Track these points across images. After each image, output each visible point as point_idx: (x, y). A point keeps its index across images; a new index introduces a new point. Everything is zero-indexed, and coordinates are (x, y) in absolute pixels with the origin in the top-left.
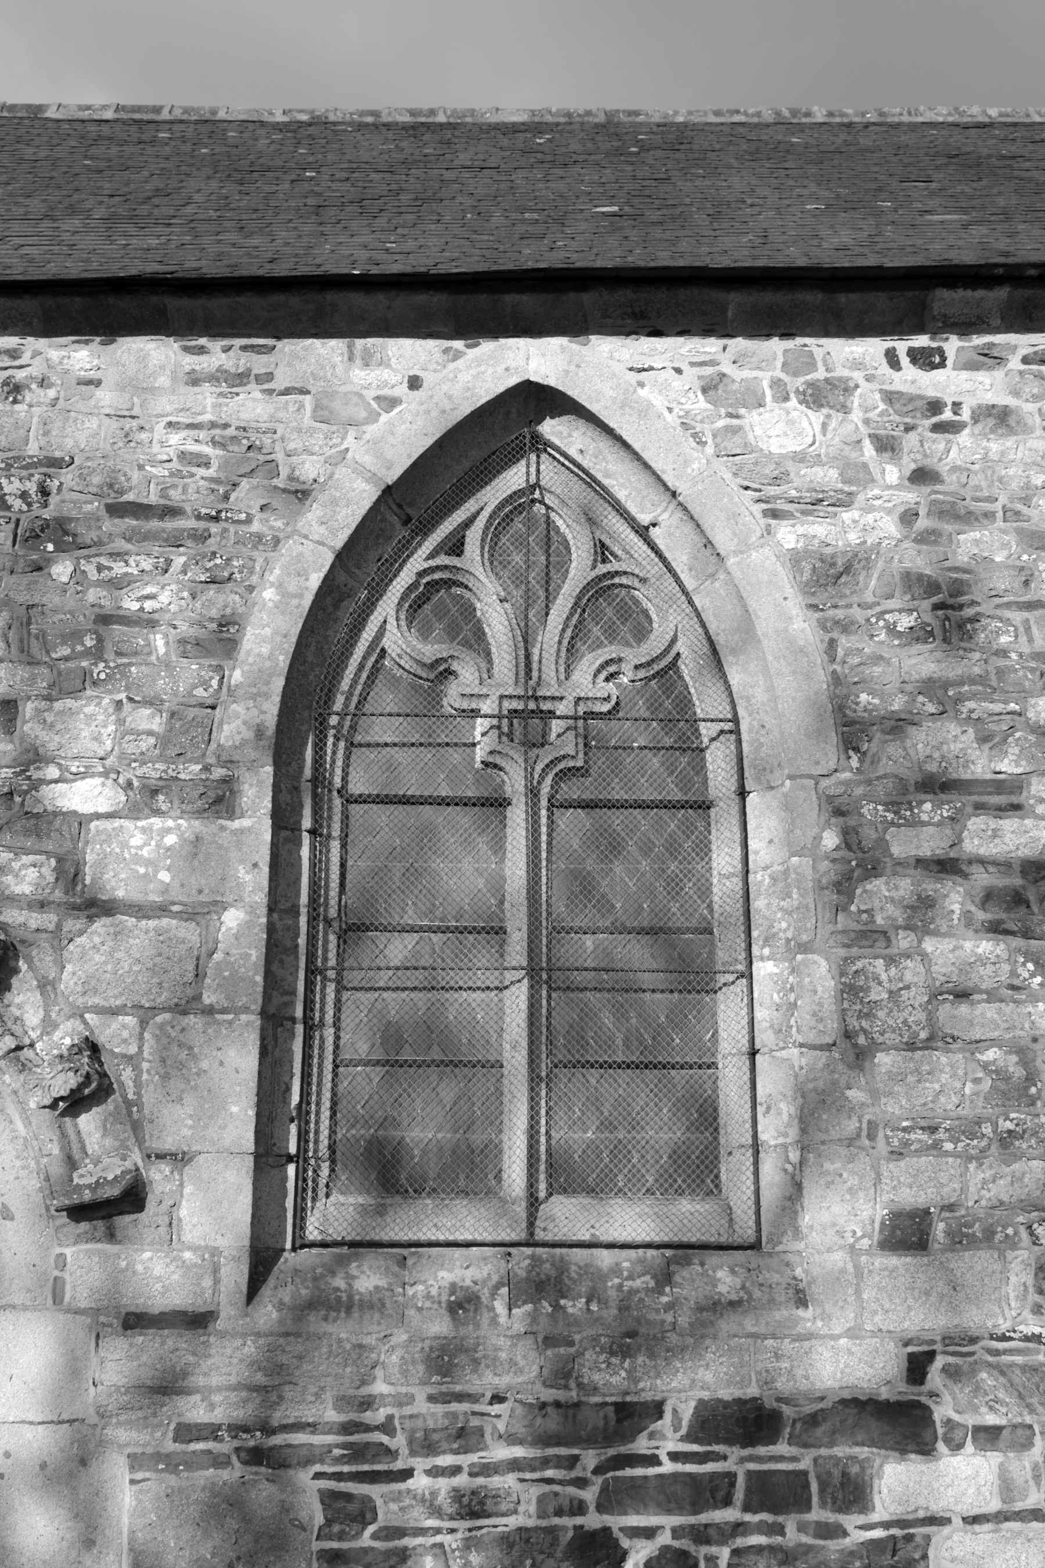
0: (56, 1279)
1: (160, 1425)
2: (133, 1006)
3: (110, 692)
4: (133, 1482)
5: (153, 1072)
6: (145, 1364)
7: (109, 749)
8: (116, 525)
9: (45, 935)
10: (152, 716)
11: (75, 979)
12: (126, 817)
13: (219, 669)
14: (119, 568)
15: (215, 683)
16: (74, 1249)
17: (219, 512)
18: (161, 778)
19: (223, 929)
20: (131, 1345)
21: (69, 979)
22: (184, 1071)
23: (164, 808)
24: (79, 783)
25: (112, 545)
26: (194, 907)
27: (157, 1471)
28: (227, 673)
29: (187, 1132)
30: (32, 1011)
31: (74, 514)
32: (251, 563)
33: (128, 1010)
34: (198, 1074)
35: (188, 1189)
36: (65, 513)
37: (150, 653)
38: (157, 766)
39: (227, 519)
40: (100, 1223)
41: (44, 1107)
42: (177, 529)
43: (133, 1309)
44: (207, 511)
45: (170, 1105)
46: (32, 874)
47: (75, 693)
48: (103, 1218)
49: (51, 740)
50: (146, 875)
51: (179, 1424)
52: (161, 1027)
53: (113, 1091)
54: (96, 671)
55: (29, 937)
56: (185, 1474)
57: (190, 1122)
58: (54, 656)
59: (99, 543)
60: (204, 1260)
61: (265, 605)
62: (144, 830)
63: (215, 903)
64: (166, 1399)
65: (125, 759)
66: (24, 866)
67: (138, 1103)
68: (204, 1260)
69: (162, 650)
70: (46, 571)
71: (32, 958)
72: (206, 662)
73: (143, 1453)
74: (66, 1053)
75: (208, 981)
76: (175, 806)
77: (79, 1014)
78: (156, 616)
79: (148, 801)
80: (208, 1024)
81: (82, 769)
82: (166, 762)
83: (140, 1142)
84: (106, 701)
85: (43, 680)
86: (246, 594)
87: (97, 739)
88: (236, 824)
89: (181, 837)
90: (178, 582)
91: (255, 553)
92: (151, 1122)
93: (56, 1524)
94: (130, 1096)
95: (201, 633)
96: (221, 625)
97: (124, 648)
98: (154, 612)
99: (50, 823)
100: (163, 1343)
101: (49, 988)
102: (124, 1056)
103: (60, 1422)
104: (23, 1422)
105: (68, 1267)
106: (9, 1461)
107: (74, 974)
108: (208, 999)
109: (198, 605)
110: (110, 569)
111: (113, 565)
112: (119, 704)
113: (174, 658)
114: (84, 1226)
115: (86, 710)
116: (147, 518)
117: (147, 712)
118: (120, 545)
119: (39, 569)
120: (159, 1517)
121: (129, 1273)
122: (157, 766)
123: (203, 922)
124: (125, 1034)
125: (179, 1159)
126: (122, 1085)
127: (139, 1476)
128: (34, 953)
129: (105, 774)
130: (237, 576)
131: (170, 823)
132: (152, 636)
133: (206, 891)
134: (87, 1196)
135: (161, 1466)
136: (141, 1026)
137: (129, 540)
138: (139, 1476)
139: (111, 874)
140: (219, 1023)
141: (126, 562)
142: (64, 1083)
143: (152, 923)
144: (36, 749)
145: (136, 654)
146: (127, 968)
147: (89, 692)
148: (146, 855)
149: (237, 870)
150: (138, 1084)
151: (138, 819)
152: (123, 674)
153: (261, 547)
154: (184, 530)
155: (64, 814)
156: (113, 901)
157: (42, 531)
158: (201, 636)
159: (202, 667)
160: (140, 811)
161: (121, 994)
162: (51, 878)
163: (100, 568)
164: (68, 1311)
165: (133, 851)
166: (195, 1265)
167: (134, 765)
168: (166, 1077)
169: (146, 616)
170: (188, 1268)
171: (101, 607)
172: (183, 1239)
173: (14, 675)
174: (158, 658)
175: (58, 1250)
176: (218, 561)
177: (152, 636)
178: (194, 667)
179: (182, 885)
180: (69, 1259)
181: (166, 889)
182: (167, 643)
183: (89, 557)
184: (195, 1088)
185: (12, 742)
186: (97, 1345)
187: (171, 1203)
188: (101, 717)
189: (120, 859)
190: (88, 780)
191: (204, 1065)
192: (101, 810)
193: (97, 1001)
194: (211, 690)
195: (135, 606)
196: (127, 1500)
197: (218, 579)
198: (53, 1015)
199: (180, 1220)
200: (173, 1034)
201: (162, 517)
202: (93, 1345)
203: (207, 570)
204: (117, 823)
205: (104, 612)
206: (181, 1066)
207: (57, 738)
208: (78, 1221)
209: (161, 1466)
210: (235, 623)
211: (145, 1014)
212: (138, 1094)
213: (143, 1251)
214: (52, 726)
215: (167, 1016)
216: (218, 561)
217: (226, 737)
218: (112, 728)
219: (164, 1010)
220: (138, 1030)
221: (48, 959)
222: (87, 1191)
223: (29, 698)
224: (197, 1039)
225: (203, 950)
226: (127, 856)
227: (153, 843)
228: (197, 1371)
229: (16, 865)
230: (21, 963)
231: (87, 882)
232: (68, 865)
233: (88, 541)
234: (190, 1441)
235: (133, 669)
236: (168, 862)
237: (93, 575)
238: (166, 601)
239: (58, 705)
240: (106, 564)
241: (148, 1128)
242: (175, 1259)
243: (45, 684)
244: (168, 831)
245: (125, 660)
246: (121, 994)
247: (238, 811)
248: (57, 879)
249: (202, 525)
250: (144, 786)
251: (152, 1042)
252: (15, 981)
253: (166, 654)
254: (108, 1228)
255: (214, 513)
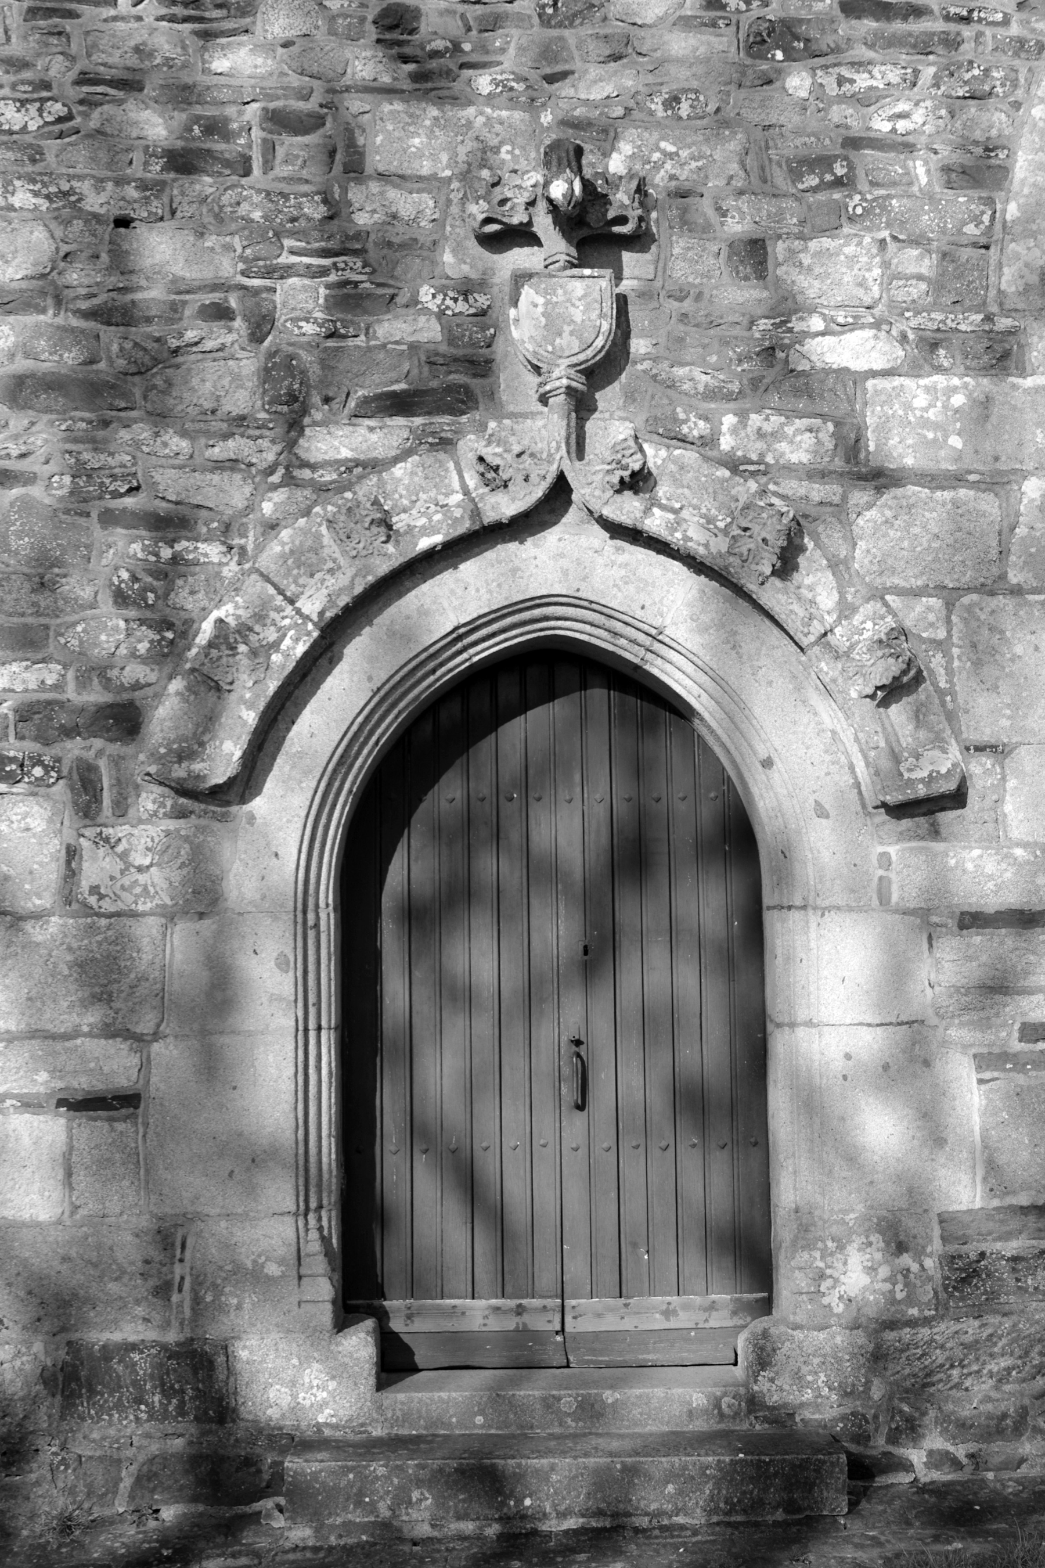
0: (881, 878)
1: (1004, 1025)
2: (936, 587)
3: (868, 229)
4: (981, 1081)
5: (964, 659)
6: (985, 964)
7: (877, 296)
8: (851, 28)
9: (829, 509)
10: (921, 257)
11: (870, 558)
12: (907, 375)
13: (990, 202)
14: (862, 81)
15: (986, 218)
16: (898, 847)
17: (971, 11)
18: (938, 330)
19: (1025, 501)
20: (968, 945)
21: (862, 557)
22: (997, 657)
23: (946, 364)
24: (848, 336)
25: (851, 52)
26: (992, 477)
27: (1005, 1070)
28: (999, 206)
29: (1005, 723)
30: (825, 593)
31: (803, 14)
32: (1013, 75)
33: (931, 591)
34: (1012, 660)
35: (1011, 783)
36: (792, 13)
37: (910, 184)
38: (933, 315)
39: (980, 20)
40: (922, 820)
41: (867, 697)
42: (925, 33)
43: (966, 909)
44: (958, 10)
45: (985, 694)
46: (808, 439)
47: (831, 230)
48: (924, 815)
49: (811, 286)
50: (935, 440)
51: (1024, 1024)
52: (969, 609)
53: (924, 680)
54: (851, 204)
55: (813, 511)
56: (1034, 1073)
57: (1008, 712)
58: (800, 186)
59: (836, 50)
60: (1036, 856)
61: (1035, 125)
62: (927, 389)
63: (1015, 471)
64: (1008, 999)
65: (899, 310)
66: (798, 431)
67: (952, 692)
68: (1036, 856)
69: (924, 180)
70: (777, 84)
71: (818, 535)
72: (975, 194)
73: (990, 1053)
74: (884, 638)
75: (1013, 558)
76: (958, 362)
77: (878, 595)
78: (910, 139)
79: (928, 356)
80: (1019, 605)
81: (850, 320)
82: (943, 311)
83: (957, 734)
84: (867, 240)
85: (792, 216)
86: (1012, 112)
87: (862, 284)
88: (1029, 382)
89: (969, 396)
90: (933, 98)
91: (1017, 62)
92: (967, 712)
93: (905, 1123)
94: (942, 685)
95: (967, 160)
96: (987, 149)
97: (881, 176)
98: (908, 134)
99: (822, 382)
100: (1002, 943)
101: (841, 567)
102: (933, 641)
103: (899, 1024)
104: (860, 1024)
105: (894, 866)
106: (850, 1063)
107: (868, 551)
108: (1014, 577)
109: (958, 124)
110: (852, 81)
111: (855, 77)
112: (883, 241)
113: (937, 189)
114: (906, 823)
115: (847, 250)
116: (888, 19)
117: (915, 252)
118: (862, 52)
119: (770, 82)
120: (1011, 1115)
121: (959, 872)
122: (933, 315)
123: (1002, 493)
124: (931, 617)
125: (995, 750)
126: (931, 672)
127: (987, 1075)
128: (820, 529)
129: (877, 325)
130: (999, 90)
131: (956, 381)
132: (910, 163)
133: (1003, 458)
134: (922, 791)
135: (1008, 1066)
136: (947, 609)
137: (871, 46)
138: (987, 1075)
139: (896, 439)
140: (1030, 604)
141: (870, 72)
142: (884, 671)
143: (947, 495)
144: (794, 296)
145: (894, 184)
146: (925, 545)
147: (847, 230)
148: (933, 418)
149: (1034, 434)
150: (950, 672)
151: (919, 376)
152: (883, 208)
153: (1023, 55)
154: (934, 34)
155: (835, 371)
156: (903, 469)
157: (769, 35)
158: (966, 163)
159: (971, 200)
160: (921, 367)
161: (922, 574)
162: (829, 445)
163: (841, 81)
164: (896, 911)
165: (918, 413)
166: (1028, 862)
167: (907, 314)
168: (978, 664)
169: (900, 139)
170: (1020, 865)
171: (847, 127)
172: (1010, 835)
173: (759, 210)
174: (920, 190)
175: (880, 849)
176: (976, 72)
177: (910, 163)
178: (961, 199)
179: (976, 452)
180: (894, 858)
181: (959, 457)
182: (928, 171)
183: (827, 67)
184: (1010, 675)
185: (766, 288)
186: (931, 945)
187: (995, 797)
188: (864, 259)
189: (905, 423)
190: (857, 333)
191: (1018, 650)
192: (877, 366)
193: (896, 582)
194: (982, 227)
195: (886, 127)
196: (976, 1099)
197: (978, 94)
198: (849, 597)
199: (1005, 815)
200: (983, 617)
201: (905, 18)
202: (925, 946)
203: (966, 83)
204: (897, 381)
205: (852, 134)
206: (993, 651)
207: (816, 284)
208: (899, 818)
209: (1008, 1066)
210: (1004, 148)
211: (950, 596)
212: (950, 681)
213: (971, 848)
214: (810, 269)
215: (975, 597)
216: (976, 72)
217: (1008, 282)
218: (877, 272)
219: (969, 590)
220: (944, 612)
221: (836, 535)
222: (921, 786)
223: (779, 237)
224: (1008, 623)
225: (1005, 524)
226: (912, 419)
227: (939, 404)
228: (1038, 970)
229: (789, 430)
230: (806, 540)
231: (872, 448)
232: (846, 429)
233: (824, 48)
234: (1037, 1040)
235: (894, 202)
236: (958, 425)
237: (832, 89)
238: (920, 121)
239: (813, 245)
240: (848, 75)
241: (963, 719)
242: (1007, 856)
243: (795, 220)
244: (955, 390)
245: (882, 192)
246: (922, 574)
247: (1029, 368)
248: (836, 445)
249: (952, 27)
250: (921, 339)
251: (961, 626)
252: (802, 560)
253: (929, 183)
254: (932, 825)
255: (965, 13)
